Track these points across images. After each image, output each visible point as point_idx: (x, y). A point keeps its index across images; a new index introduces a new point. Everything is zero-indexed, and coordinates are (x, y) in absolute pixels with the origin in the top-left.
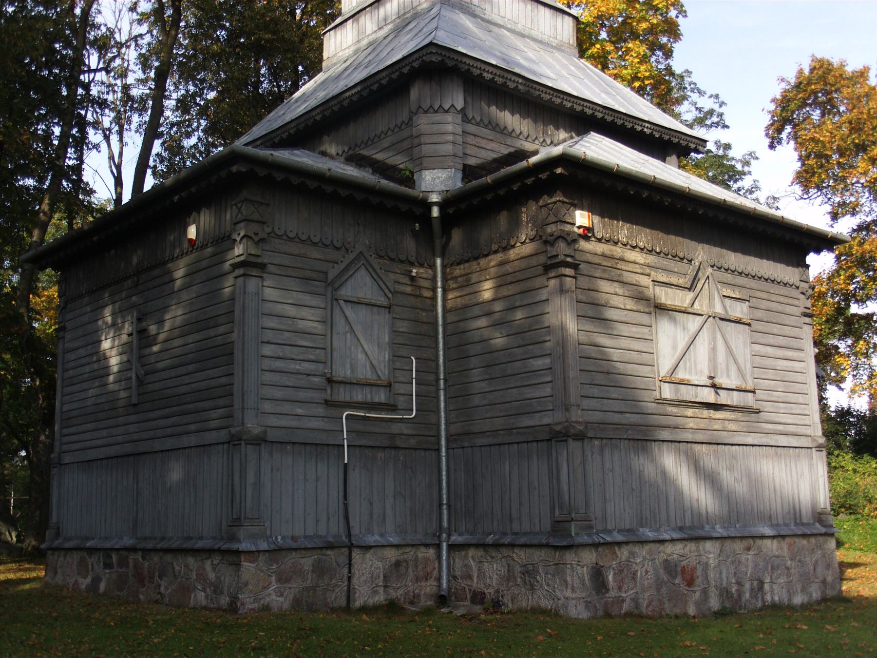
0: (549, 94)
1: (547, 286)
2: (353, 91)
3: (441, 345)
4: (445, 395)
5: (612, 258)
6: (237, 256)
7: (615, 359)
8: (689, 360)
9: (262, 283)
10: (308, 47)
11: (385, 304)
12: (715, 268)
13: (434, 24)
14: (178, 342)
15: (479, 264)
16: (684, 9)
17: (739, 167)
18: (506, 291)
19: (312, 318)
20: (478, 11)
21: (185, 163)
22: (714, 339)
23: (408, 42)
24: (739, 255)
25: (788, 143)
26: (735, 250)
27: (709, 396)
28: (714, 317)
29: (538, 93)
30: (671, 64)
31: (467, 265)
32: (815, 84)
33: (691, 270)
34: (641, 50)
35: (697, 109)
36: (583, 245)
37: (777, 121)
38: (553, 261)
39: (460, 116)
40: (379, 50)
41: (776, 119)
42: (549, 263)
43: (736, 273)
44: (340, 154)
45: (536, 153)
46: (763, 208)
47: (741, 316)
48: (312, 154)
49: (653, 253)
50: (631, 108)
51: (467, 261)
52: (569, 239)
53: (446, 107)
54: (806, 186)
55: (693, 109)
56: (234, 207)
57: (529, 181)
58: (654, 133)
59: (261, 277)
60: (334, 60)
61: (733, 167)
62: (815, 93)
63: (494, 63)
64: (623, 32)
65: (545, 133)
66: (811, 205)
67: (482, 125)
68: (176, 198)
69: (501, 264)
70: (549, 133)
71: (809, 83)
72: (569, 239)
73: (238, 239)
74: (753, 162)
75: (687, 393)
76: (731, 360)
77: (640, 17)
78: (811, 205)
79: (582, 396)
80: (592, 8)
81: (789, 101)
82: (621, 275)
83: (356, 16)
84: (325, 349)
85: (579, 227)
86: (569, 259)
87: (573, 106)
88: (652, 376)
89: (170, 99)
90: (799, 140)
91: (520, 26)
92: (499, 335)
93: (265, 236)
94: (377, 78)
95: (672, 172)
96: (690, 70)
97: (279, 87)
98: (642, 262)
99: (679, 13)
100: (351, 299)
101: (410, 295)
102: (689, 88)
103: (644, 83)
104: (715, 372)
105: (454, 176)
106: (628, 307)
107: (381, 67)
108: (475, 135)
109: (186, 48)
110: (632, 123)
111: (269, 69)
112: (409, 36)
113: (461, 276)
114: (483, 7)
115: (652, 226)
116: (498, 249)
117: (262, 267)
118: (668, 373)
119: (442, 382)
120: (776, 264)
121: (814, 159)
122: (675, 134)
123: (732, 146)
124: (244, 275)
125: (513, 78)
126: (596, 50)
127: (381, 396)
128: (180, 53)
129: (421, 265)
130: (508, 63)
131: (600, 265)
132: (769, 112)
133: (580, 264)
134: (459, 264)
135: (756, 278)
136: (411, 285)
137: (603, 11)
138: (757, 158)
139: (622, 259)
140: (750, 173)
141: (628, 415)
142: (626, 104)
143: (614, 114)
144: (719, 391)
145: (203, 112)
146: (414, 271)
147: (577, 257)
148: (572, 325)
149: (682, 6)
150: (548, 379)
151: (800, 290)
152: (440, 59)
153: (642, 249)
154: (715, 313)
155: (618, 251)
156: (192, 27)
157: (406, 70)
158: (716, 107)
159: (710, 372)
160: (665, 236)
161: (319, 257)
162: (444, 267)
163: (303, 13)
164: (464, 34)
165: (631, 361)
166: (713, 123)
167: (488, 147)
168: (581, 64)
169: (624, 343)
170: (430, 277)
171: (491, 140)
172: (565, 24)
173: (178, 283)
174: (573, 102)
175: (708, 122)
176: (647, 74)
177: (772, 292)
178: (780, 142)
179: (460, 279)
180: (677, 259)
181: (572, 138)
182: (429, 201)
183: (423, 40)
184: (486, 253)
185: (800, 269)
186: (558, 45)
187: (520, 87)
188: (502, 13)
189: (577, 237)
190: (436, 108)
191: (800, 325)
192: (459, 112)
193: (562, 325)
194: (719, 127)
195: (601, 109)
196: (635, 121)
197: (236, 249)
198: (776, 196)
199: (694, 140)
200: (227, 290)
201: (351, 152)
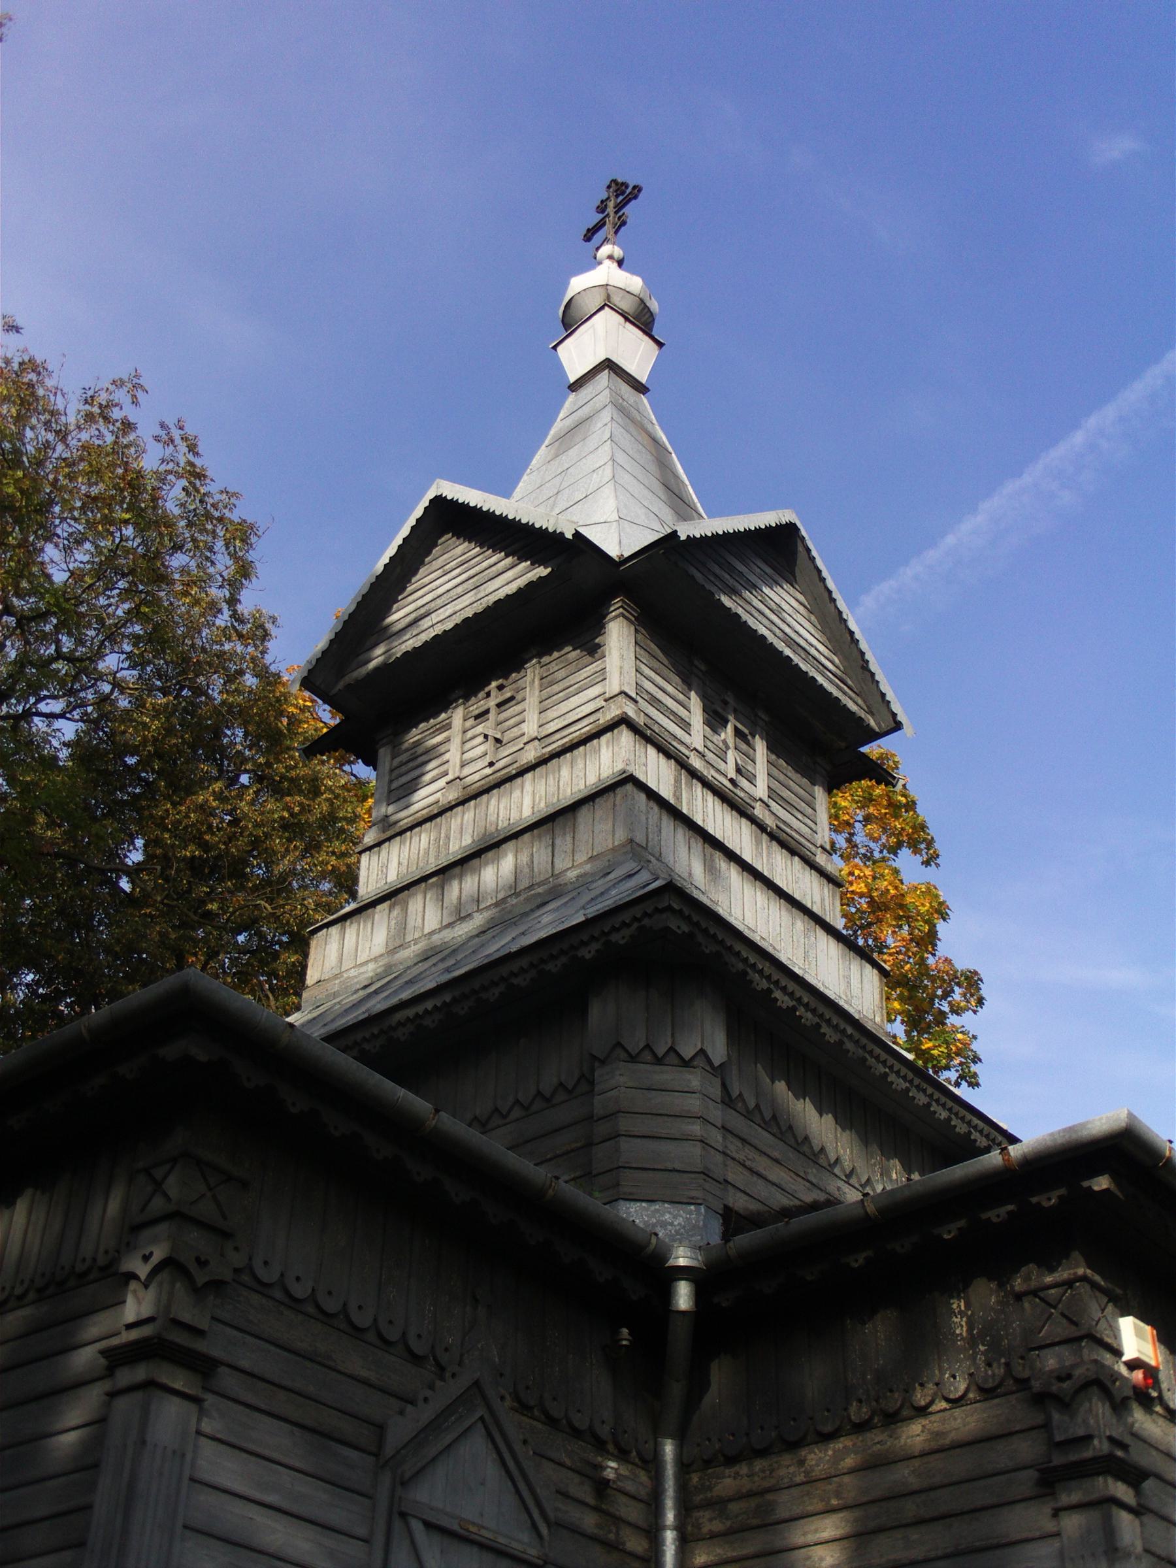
0: (904, 1078)
2: (429, 1005)
6: (129, 1327)
9: (199, 1420)
15: (802, 1462)
29: (882, 1069)
31: (759, 1464)
36: (1137, 1415)
38: (1073, 1457)
42: (1058, 1460)
51: (762, 1453)
53: (688, 1052)
57: (999, 1214)
67: (758, 1119)
85: (1134, 1365)
93: (228, 1276)
94: (504, 971)
100: (445, 1522)
101: (593, 1538)
105: (705, 1225)
116: (871, 1418)
136: (596, 1509)
152: (685, 928)
157: (588, 953)
161: (364, 1373)
162: (684, 1467)
170: (643, 1493)
172: (865, 980)
179: (734, 1507)
182: (671, 1262)
184: (828, 1428)
197: (130, 1301)
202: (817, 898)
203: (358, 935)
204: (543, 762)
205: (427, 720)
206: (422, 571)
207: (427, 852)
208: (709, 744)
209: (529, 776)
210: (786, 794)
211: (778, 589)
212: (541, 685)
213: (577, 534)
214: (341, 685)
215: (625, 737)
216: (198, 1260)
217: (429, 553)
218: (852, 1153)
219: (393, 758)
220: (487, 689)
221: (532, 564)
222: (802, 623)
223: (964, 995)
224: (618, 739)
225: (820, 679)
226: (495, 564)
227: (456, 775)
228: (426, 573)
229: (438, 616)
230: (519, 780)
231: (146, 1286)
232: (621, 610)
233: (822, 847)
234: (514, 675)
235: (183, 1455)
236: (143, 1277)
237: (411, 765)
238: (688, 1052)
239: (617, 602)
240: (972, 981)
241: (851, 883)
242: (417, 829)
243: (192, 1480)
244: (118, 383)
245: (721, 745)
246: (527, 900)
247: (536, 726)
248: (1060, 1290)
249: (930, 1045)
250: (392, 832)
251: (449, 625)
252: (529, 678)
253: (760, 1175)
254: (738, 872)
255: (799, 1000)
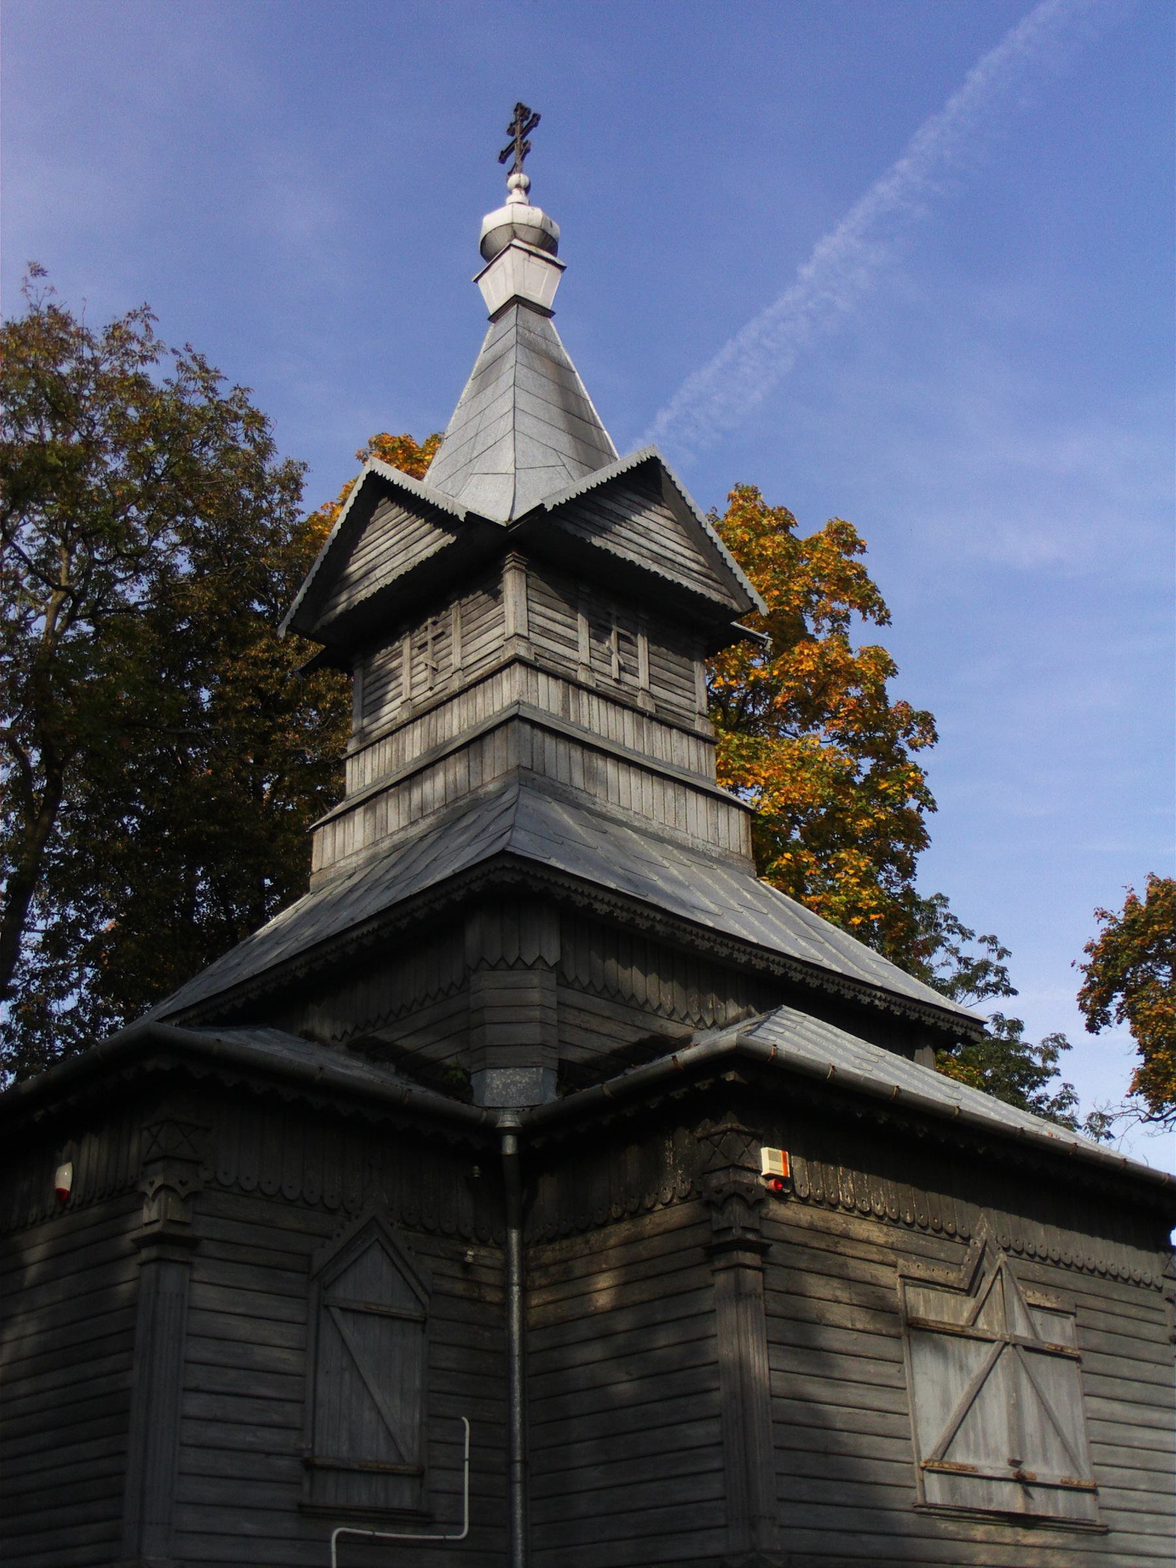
0: (709, 940)
1: (712, 1285)
2: (365, 930)
3: (517, 1394)
4: (524, 1492)
5: (827, 1233)
6: (147, 1224)
7: (839, 1425)
8: (974, 1429)
10: (282, 847)
11: (416, 1315)
12: (1011, 1252)
13: (507, 820)
14: (24, 1387)
15: (587, 1242)
16: (930, 797)
17: (1037, 1061)
18: (638, 1293)
19: (278, 1342)
20: (583, 798)
21: (52, 1042)
22: (1016, 1388)
23: (462, 848)
24: (1053, 1228)
25: (1119, 1022)
26: (1043, 1219)
27: (1010, 1499)
28: (1014, 1346)
30: (912, 886)
31: (565, 1243)
32: (1159, 923)
33: (968, 1257)
34: (862, 864)
35: (960, 960)
36: (777, 1209)
37: (1099, 984)
38: (722, 1240)
39: (553, 976)
40: (411, 859)
41: (1096, 979)
42: (715, 1241)
43: (1049, 1262)
44: (339, 1037)
45: (686, 1042)
46: (1084, 1139)
47: (1061, 1343)
48: (288, 1036)
49: (901, 1224)
50: (850, 964)
51: (567, 1236)
52: (750, 1198)
54: (1156, 1097)
55: (954, 960)
56: (145, 1134)
57: (678, 1094)
58: (892, 1008)
59: (189, 1264)
60: (332, 874)
61: (1028, 1060)
62: (1159, 937)
63: (613, 886)
64: (829, 832)
65: (702, 1006)
66: (1167, 1130)
68: (38, 1115)
69: (628, 1242)
70: (710, 1006)
71: (1149, 922)
72: (750, 1198)
73: (150, 1193)
74: (1061, 1052)
75: (973, 1495)
76: (1050, 1430)
77: (857, 810)
78: (1167, 1130)
79: (780, 1500)
80: (776, 794)
81: (1116, 950)
82: (845, 1265)
83: (371, 802)
84: (302, 1402)
85: (768, 1177)
86: (750, 1236)
87: (750, 960)
88: (908, 1459)
89: (34, 931)
90: (1139, 1017)
91: (655, 823)
92: (625, 1377)
95: (926, 1078)
96: (944, 895)
97: (229, 913)
98: (881, 1240)
99: (923, 803)
100: (354, 1306)
101: (462, 1297)
102: (944, 926)
103: (868, 918)
104: (1021, 1454)
106: (859, 1326)
107: (415, 890)
108: (580, 1010)
109: (67, 845)
110: (854, 990)
111: (212, 883)
112: (463, 838)
113: (555, 1263)
114: (592, 791)
115: (897, 1176)
116: (623, 1214)
117: (191, 1244)
118: (935, 1453)
119: (518, 1468)
120: (1118, 1244)
121: (1167, 1049)
122: (929, 1010)
123: (1025, 1026)
124: (158, 1260)
125: (646, 912)
126: (784, 862)
127: (404, 1497)
128: (54, 852)
129: (483, 1243)
130: (637, 886)
131: (805, 1246)
132: (1084, 968)
133: (769, 1246)
134: (551, 1241)
135: (1085, 1270)
137: (795, 799)
138: (1068, 1047)
139: (846, 1236)
140: (1056, 1072)
141: (865, 1538)
142: (843, 957)
143: (821, 975)
144: (1031, 1489)
145: (91, 954)
146: (470, 1253)
147: (766, 1231)
148: (759, 1361)
149: (928, 793)
150: (716, 1465)
151: (1164, 1294)
152: (518, 878)
153: (880, 1218)
154: (1016, 1337)
155: (837, 1221)
156: (79, 809)
157: (458, 896)
158: (992, 958)
159: (1012, 1450)
160: (920, 1193)
162: (523, 1245)
163: (275, 791)
164: (560, 837)
165: (868, 1430)
166: (988, 984)
167: (602, 1030)
168: (761, 888)
169: (853, 1394)
171: (608, 1018)
173: (32, 1273)
174: (750, 954)
175: (980, 984)
176: (874, 903)
177: (1115, 1297)
178: (1106, 1021)
179: (552, 1270)
180: (943, 1235)
181: (749, 1015)
182: (499, 1125)
183: (493, 842)
185: (1163, 1255)
186: (720, 855)
187: (659, 927)
188: (624, 803)
189: (763, 1194)
190: (511, 961)
191: (1167, 1360)
192: (551, 969)
193: (740, 1358)
194: (1000, 993)
195: (799, 967)
196: (858, 987)
197: (145, 1210)
198: (1107, 1113)
199: (961, 1021)
200: (124, 1288)
201: (358, 1034)
202: (694, 759)
203: (344, 832)
204: (464, 690)
205: (386, 647)
206: (369, 529)
207: (391, 761)
208: (595, 654)
209: (456, 701)
210: (667, 676)
211: (647, 513)
212: (462, 623)
213: (469, 514)
214: (318, 626)
215: (519, 672)
216: (181, 1182)
217: (372, 514)
218: (673, 997)
219: (364, 679)
220: (425, 625)
221: (443, 531)
222: (669, 536)
223: (921, 732)
224: (514, 674)
225: (685, 582)
226: (418, 529)
227: (408, 696)
228: (372, 531)
229: (381, 571)
230: (449, 704)
231: (154, 1201)
232: (513, 563)
233: (700, 713)
234: (444, 612)
235: (183, 1296)
236: (150, 1195)
237: (377, 684)
238: (529, 959)
239: (509, 561)
240: (926, 720)
241: (801, 662)
242: (383, 742)
243: (190, 1308)
244: (132, 316)
245: (606, 652)
246: (453, 810)
247: (459, 659)
248: (721, 1136)
249: (885, 785)
250: (368, 743)
251: (389, 581)
252: (453, 617)
253: (592, 1031)
254: (614, 765)
255: (615, 905)
